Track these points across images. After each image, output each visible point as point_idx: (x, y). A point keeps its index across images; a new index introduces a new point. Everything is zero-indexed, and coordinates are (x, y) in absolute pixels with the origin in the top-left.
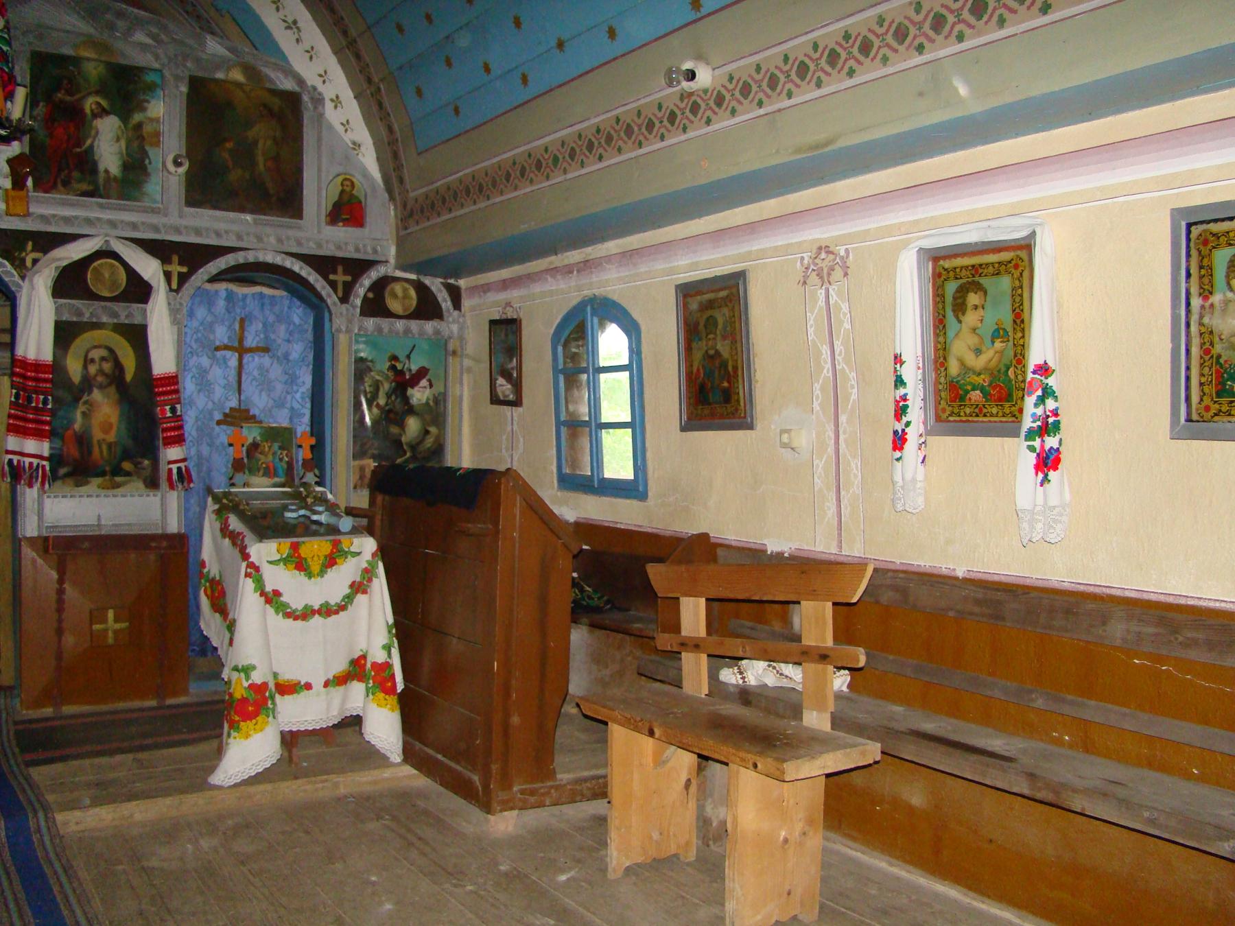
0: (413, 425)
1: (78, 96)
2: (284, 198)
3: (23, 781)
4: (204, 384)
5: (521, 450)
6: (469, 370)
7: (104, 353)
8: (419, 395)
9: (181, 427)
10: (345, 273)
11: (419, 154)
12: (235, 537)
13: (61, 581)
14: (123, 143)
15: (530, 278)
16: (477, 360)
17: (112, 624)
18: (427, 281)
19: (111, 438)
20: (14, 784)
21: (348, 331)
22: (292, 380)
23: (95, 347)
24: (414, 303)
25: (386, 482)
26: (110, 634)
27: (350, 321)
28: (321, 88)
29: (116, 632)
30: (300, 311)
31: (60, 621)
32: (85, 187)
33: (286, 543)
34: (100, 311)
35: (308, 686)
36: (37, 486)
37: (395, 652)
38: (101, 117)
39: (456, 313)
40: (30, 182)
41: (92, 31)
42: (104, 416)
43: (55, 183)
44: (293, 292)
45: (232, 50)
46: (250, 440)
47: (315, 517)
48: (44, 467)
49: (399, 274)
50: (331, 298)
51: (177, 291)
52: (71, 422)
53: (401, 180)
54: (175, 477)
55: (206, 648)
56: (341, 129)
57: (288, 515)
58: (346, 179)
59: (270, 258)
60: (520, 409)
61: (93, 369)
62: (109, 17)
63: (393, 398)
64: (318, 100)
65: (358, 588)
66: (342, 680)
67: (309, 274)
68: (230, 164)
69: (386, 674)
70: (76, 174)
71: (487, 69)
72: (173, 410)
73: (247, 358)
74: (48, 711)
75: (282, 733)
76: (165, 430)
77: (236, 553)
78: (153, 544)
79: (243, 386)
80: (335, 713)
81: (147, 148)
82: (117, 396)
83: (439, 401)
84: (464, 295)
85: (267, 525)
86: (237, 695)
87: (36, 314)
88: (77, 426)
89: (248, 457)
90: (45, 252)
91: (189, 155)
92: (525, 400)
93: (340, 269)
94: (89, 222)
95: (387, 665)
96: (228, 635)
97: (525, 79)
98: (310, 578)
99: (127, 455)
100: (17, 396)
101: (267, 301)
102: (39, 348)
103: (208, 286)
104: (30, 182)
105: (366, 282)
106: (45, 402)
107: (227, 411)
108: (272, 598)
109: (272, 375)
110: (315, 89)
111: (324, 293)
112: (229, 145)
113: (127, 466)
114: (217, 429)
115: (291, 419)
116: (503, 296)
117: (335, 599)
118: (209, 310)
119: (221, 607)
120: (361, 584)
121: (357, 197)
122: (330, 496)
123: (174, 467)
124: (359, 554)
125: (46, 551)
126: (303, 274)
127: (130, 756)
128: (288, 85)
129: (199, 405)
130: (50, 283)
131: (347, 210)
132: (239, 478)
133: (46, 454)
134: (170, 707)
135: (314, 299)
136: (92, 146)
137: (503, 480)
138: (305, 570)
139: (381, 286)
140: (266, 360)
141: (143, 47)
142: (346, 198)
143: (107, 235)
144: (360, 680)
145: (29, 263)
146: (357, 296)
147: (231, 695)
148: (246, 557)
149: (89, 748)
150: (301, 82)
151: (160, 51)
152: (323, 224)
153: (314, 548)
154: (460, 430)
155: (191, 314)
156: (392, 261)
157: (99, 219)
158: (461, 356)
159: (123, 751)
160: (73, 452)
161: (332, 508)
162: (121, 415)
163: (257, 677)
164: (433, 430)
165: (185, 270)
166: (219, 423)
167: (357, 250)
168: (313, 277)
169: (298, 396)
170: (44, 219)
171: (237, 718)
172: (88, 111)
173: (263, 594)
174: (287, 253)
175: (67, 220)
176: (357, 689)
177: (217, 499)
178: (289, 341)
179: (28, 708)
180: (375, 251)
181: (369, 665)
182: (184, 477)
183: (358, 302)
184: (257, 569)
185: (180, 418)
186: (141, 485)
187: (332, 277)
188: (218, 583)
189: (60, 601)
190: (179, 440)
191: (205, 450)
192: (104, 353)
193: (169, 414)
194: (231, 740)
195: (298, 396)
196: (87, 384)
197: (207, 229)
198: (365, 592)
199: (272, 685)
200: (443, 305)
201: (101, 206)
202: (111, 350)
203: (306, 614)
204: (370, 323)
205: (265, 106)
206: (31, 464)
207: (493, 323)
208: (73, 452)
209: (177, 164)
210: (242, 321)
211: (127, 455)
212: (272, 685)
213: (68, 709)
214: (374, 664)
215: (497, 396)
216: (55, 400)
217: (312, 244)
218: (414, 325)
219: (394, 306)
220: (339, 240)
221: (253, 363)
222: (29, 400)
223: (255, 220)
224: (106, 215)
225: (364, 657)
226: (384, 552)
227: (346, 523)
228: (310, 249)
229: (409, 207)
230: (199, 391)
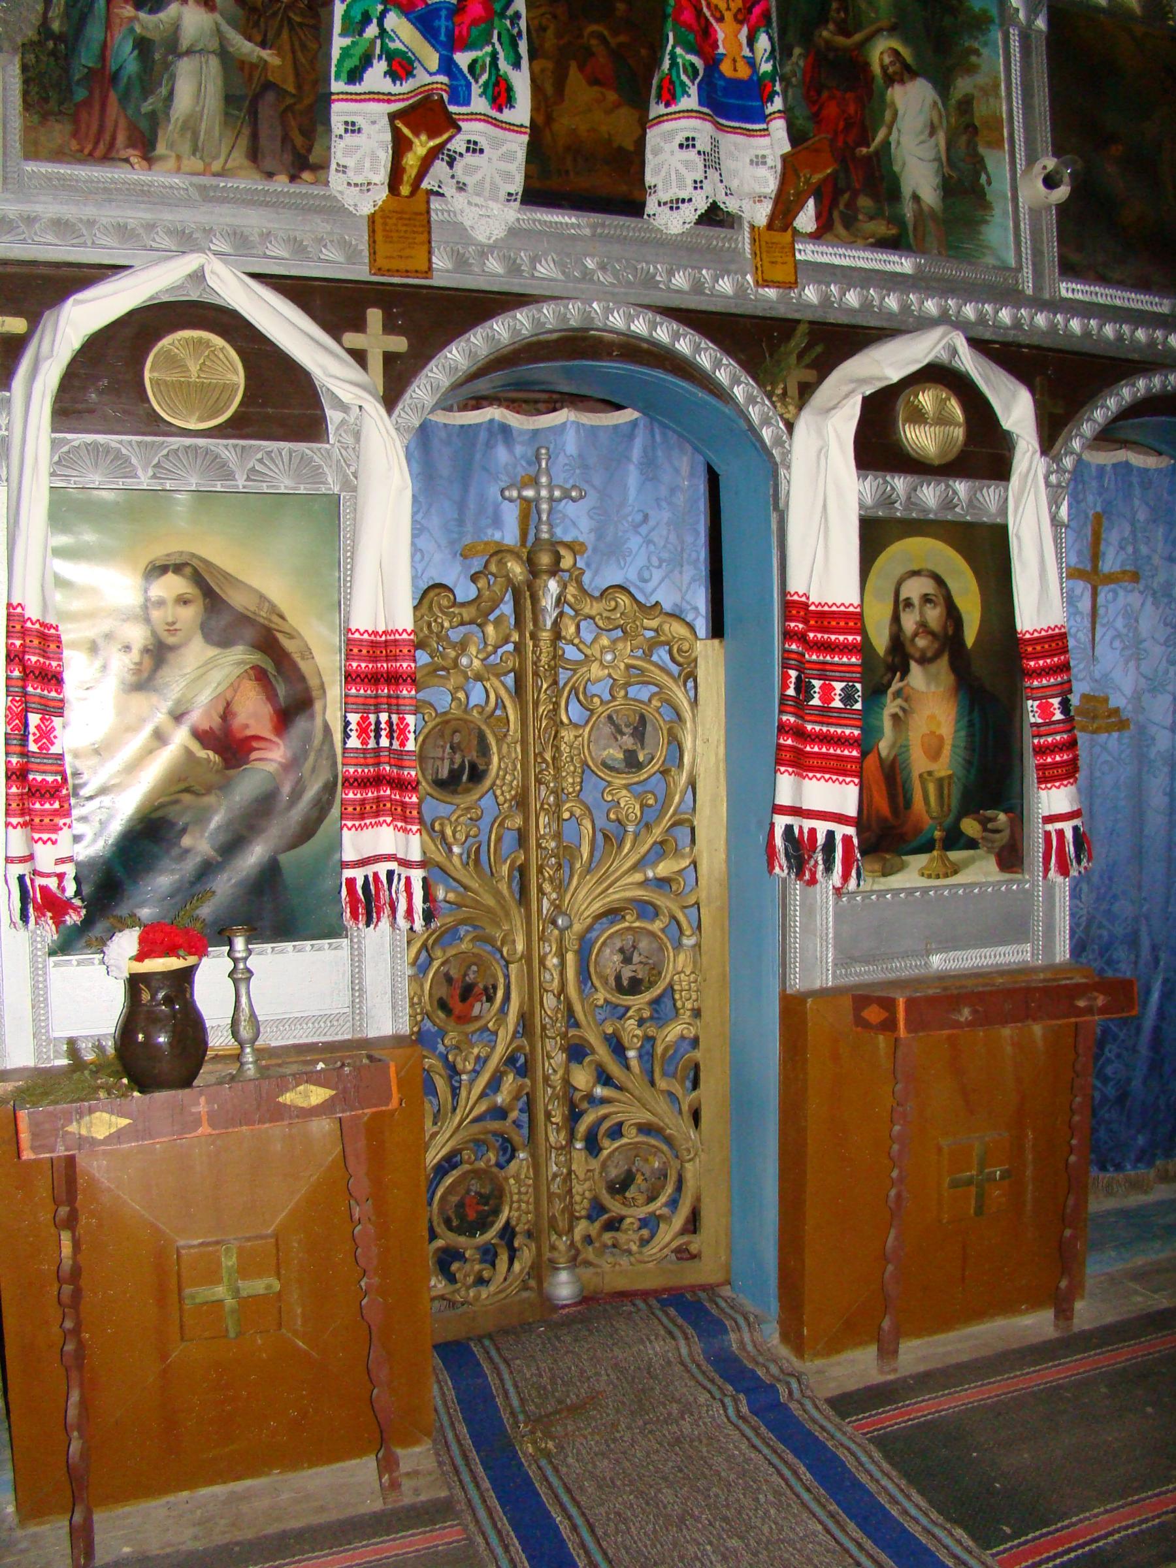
1: (858, 37)
10: (389, 327)
14: (941, 137)
23: (916, 573)
32: (881, 228)
38: (902, 82)
42: (929, 721)
70: (864, 202)
76: (1040, 751)
81: (982, 150)
93: (374, 316)
136: (886, 144)
172: (877, 69)
193: (1058, 716)
196: (900, 656)
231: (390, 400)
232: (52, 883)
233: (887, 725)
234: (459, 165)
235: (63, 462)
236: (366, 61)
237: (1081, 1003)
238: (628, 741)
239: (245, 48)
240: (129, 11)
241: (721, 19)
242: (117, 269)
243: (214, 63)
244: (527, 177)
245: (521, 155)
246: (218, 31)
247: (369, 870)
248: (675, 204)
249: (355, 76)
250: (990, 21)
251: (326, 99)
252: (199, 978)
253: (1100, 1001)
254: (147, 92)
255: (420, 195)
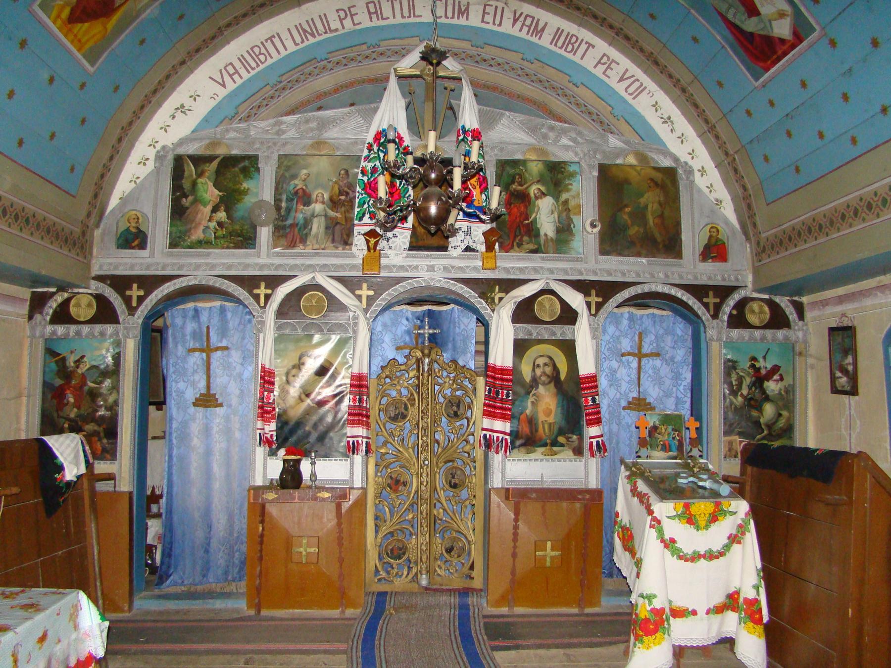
0: (769, 410)
1: (525, 186)
2: (669, 244)
3: (490, 662)
4: (614, 381)
5: (858, 430)
6: (812, 366)
7: (546, 360)
8: (772, 386)
9: (599, 412)
11: (768, 205)
12: (641, 497)
13: (516, 520)
15: (863, 294)
16: (819, 359)
17: (550, 552)
18: (777, 299)
19: (551, 419)
20: (484, 662)
21: (719, 339)
22: (677, 377)
24: (768, 316)
25: (754, 457)
26: (548, 559)
27: (719, 333)
28: (690, 162)
29: (552, 557)
30: (681, 326)
31: (515, 547)
33: (680, 504)
34: (543, 331)
35: (694, 613)
36: (502, 452)
37: (762, 591)
39: (801, 323)
40: (497, 246)
41: (533, 141)
42: (546, 406)
43: (513, 246)
44: (676, 312)
45: (627, 143)
46: (652, 424)
47: (701, 484)
48: (506, 440)
49: (755, 295)
50: (705, 315)
51: (595, 315)
52: (525, 408)
53: (755, 225)
54: (595, 448)
55: (614, 572)
56: (707, 191)
57: (680, 481)
58: (712, 227)
59: (660, 289)
60: (856, 398)
61: (538, 372)
62: (543, 130)
63: (753, 389)
64: (690, 172)
65: (734, 539)
66: (719, 610)
67: (689, 299)
68: (629, 222)
69: (755, 608)
70: (526, 238)
71: (821, 135)
72: (594, 400)
73: (644, 361)
74: (504, 610)
75: (674, 646)
76: (587, 415)
77: (643, 509)
78: (580, 497)
79: (641, 382)
80: (714, 635)
82: (555, 390)
83: (790, 391)
84: (806, 309)
85: (666, 489)
86: (642, 616)
87: (502, 336)
88: (528, 412)
89: (650, 436)
90: (507, 293)
91: (601, 218)
92: (860, 391)
94: (536, 270)
95: (756, 601)
96: (635, 569)
97: (854, 141)
98: (698, 530)
99: (561, 432)
100: (490, 391)
101: (657, 319)
102: (503, 358)
103: (616, 310)
104: (497, 246)
105: (731, 302)
106: (508, 396)
107: (630, 400)
108: (669, 544)
109: (662, 373)
110: (686, 163)
111: (700, 312)
112: (627, 210)
113: (561, 439)
114: (623, 413)
115: (676, 405)
116: (839, 309)
117: (716, 547)
118: (617, 327)
119: (630, 548)
120: (736, 536)
121: (721, 240)
122: (710, 467)
123: (594, 441)
124: (735, 513)
125: (507, 498)
126: (684, 299)
127: (561, 651)
128: (666, 163)
129: (610, 396)
130: (510, 313)
131: (715, 250)
132: (644, 452)
133: (508, 431)
134: (587, 615)
135: (692, 317)
136: (535, 219)
137: (856, 460)
138: (693, 524)
139: (741, 305)
140: (658, 362)
141: (567, 148)
142: (713, 241)
143: (547, 279)
144: (733, 610)
145: (496, 301)
146: (724, 313)
147: (636, 615)
148: (651, 512)
149: (531, 642)
150: (676, 160)
151: (578, 150)
152: (697, 260)
153: (702, 508)
154: (806, 413)
155: (604, 331)
156: (750, 285)
157: (542, 268)
158: (806, 356)
159: (557, 646)
160: (525, 429)
161: (712, 475)
162: (558, 403)
163: (657, 604)
164: (785, 413)
165: (600, 300)
166: (624, 408)
167: (724, 279)
168: (691, 301)
169: (681, 388)
170: (507, 270)
171: (641, 633)
172: (532, 195)
173: (663, 541)
174: (671, 284)
175: (521, 270)
176: (731, 619)
177: (627, 467)
178: (674, 348)
179: (492, 606)
180: (737, 280)
181: (741, 600)
182: (601, 448)
183: (726, 318)
184: (659, 522)
185: (598, 406)
186: (571, 453)
187: (705, 300)
188: (628, 529)
189: (515, 535)
190: (598, 421)
191: (615, 428)
192: (546, 360)
193: (591, 403)
194: (636, 649)
195: (681, 388)
196: (535, 382)
197: (615, 270)
198: (739, 543)
199: (667, 610)
200: (790, 317)
201: (543, 259)
202: (551, 358)
203: (694, 558)
204: (735, 333)
205: (652, 180)
206: (498, 437)
207: (832, 330)
208: (525, 429)
209: (593, 226)
210: (640, 334)
211: (561, 432)
212: (667, 610)
213: (519, 610)
214: (746, 600)
215: (836, 387)
216: (514, 394)
217: (690, 277)
218: (769, 333)
219: (752, 319)
220: (709, 273)
221: (648, 364)
222: (497, 393)
223: (648, 262)
224: (548, 265)
225: (737, 593)
226: (755, 512)
227: (725, 489)
228: (689, 280)
229: (762, 244)
230: (611, 385)
231: (366, 311)
232: (269, 436)
233: (529, 404)
234: (390, 241)
235: (279, 328)
236: (364, 215)
237: (580, 497)
238: (455, 408)
239: (332, 214)
240: (302, 207)
241: (475, 188)
242: (295, 276)
243: (323, 219)
244: (411, 242)
245: (409, 237)
246: (325, 210)
247: (355, 439)
248: (455, 247)
249: (361, 219)
250: (577, 173)
251: (354, 225)
252: (302, 462)
253: (588, 497)
254: (305, 228)
255: (377, 252)
